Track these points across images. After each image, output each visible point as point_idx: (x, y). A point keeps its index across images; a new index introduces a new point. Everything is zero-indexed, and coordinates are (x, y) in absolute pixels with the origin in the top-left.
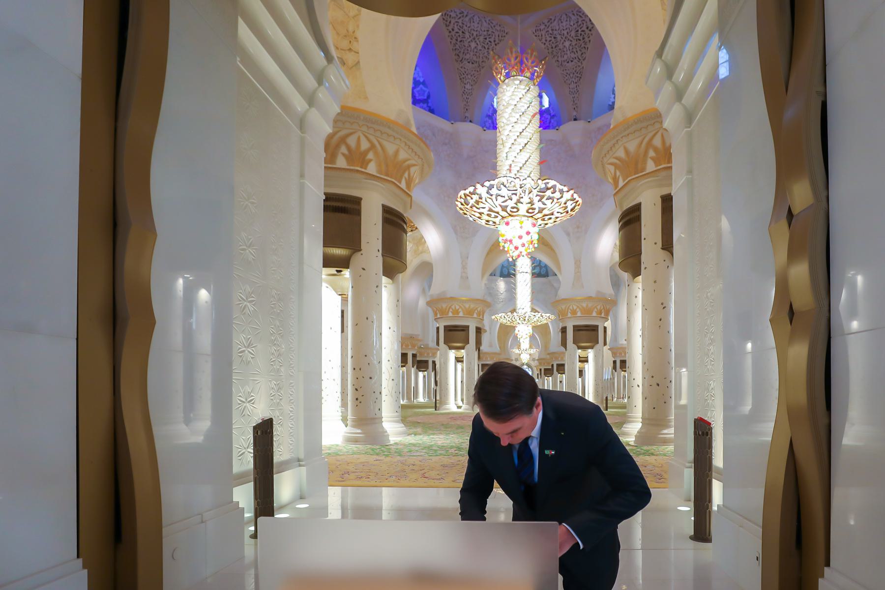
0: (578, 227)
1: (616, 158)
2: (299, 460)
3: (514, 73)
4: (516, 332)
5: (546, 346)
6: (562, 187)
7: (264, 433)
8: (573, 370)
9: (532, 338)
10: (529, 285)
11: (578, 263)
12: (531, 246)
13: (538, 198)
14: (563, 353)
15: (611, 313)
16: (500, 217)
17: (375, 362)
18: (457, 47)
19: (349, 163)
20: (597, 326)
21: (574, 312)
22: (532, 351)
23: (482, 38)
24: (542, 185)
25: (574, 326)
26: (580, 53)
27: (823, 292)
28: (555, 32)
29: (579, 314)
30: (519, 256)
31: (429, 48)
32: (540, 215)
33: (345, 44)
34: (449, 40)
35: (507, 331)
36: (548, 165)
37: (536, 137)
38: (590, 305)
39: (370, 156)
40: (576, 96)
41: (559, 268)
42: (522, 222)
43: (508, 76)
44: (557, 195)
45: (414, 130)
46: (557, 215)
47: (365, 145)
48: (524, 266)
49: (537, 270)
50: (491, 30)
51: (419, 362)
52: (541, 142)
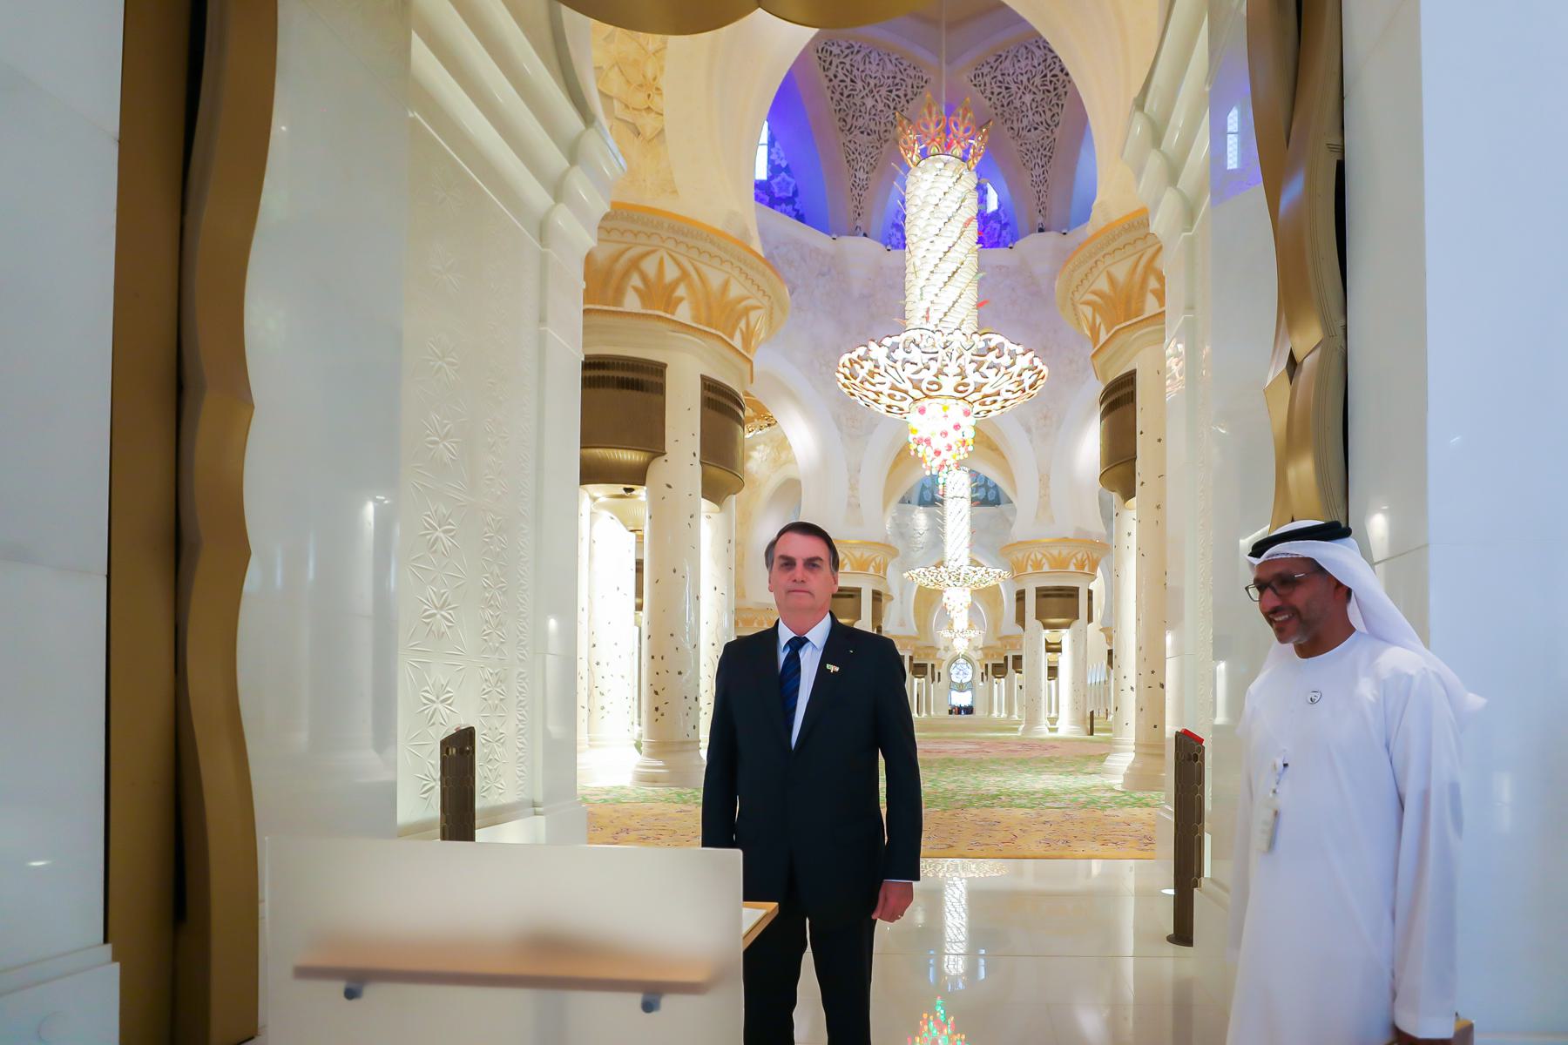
0: (1045, 417)
1: (1094, 293)
2: (534, 805)
3: (934, 150)
4: (945, 600)
5: (995, 624)
6: (1013, 347)
7: (459, 754)
8: (1036, 664)
9: (972, 608)
10: (967, 519)
11: (1044, 480)
12: (962, 450)
13: (974, 366)
14: (1020, 637)
15: (1102, 562)
16: (910, 400)
17: (689, 647)
18: (843, 106)
19: (644, 305)
20: (1077, 589)
21: (1038, 565)
22: (972, 634)
23: (883, 91)
24: (979, 343)
25: (1038, 590)
26: (1049, 114)
27: (1339, 498)
28: (1007, 79)
29: (1046, 568)
30: (942, 466)
31: (787, 106)
32: (977, 396)
33: (639, 99)
34: (829, 94)
35: (929, 599)
36: (989, 312)
37: (972, 261)
38: (1065, 552)
39: (681, 291)
40: (1043, 188)
41: (1015, 491)
42: (945, 408)
43: (924, 155)
44: (1006, 360)
45: (757, 246)
46: (1005, 395)
47: (671, 273)
48: (957, 487)
49: (981, 494)
50: (899, 76)
51: (917, 666)
52: (980, 268)
